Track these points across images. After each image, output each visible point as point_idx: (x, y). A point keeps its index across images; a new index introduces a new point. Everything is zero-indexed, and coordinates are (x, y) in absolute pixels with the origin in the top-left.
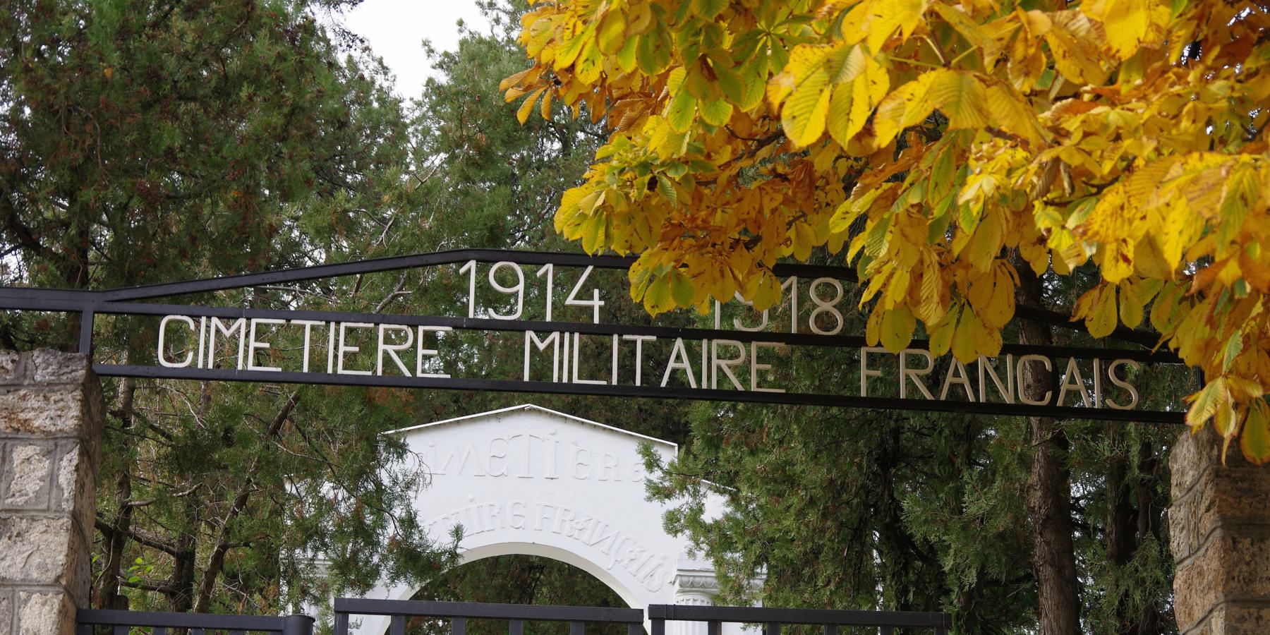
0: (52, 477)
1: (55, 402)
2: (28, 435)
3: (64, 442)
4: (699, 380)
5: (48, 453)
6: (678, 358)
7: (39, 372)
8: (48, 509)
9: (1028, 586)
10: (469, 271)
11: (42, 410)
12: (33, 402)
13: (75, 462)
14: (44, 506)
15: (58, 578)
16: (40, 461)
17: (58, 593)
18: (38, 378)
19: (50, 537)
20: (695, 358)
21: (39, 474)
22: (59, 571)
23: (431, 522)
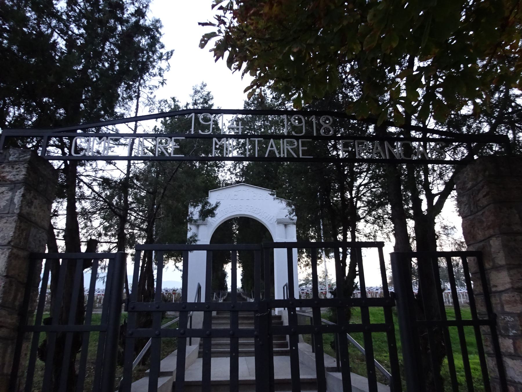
0: (12, 199)
1: (17, 169)
2: (4, 183)
3: (18, 184)
4: (279, 153)
5: (11, 190)
6: (272, 146)
7: (11, 157)
8: (8, 213)
9: (378, 228)
10: (192, 117)
11: (10, 172)
12: (7, 169)
13: (22, 193)
14: (6, 212)
15: (9, 243)
16: (7, 193)
17: (9, 249)
18: (10, 159)
19: (8, 225)
20: (277, 144)
21: (6, 198)
22: (10, 239)
23: (284, 210)
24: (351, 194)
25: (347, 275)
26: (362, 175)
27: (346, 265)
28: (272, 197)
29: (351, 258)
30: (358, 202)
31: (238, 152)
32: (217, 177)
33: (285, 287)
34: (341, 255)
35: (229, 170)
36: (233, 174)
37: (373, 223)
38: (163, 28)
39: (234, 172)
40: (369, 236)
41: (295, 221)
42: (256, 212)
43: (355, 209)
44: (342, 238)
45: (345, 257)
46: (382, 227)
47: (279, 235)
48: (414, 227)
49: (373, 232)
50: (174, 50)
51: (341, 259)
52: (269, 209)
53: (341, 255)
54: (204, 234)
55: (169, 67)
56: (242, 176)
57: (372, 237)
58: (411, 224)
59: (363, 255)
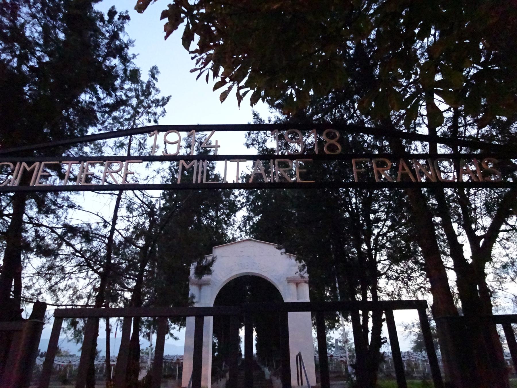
24: (368, 245)
25: (369, 343)
26: (379, 225)
27: (368, 331)
28: (279, 251)
29: (373, 321)
30: (378, 255)
31: (247, 209)
32: (226, 235)
33: (298, 357)
34: (361, 318)
35: (239, 228)
36: (243, 231)
37: (397, 279)
38: (159, 74)
39: (244, 229)
40: (392, 294)
41: (307, 279)
42: (264, 270)
43: (374, 263)
44: (361, 298)
45: (366, 321)
46: (407, 284)
47: (290, 295)
48: (456, 281)
49: (397, 290)
50: (171, 96)
51: (361, 323)
52: (278, 266)
53: (361, 318)
54: (205, 297)
55: (164, 112)
56: (251, 233)
57: (396, 297)
58: (452, 276)
59: (100, 326)
